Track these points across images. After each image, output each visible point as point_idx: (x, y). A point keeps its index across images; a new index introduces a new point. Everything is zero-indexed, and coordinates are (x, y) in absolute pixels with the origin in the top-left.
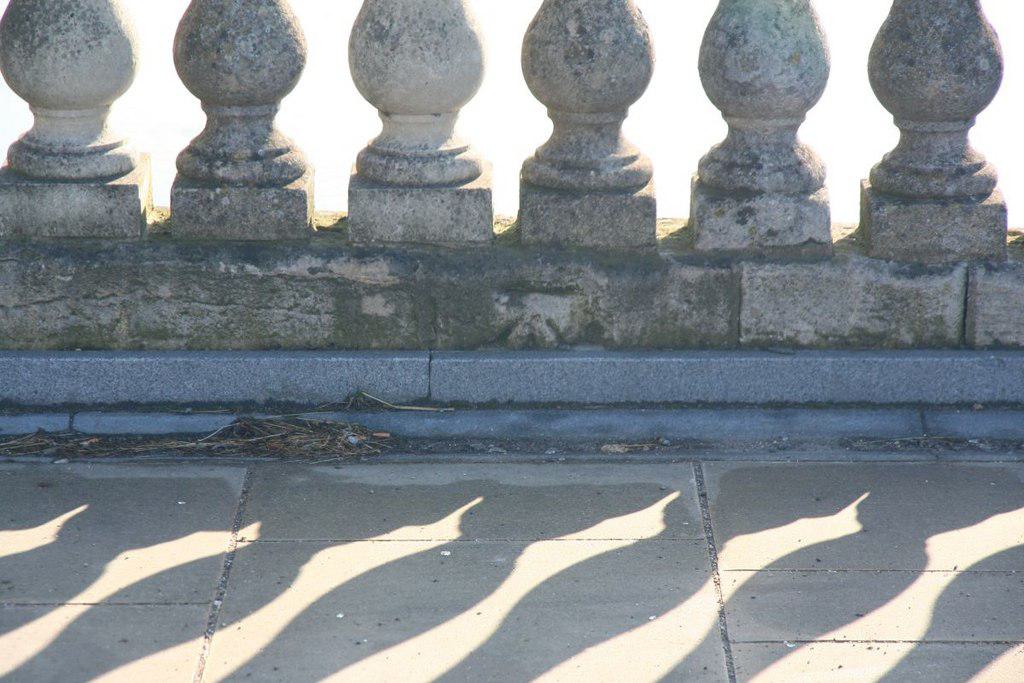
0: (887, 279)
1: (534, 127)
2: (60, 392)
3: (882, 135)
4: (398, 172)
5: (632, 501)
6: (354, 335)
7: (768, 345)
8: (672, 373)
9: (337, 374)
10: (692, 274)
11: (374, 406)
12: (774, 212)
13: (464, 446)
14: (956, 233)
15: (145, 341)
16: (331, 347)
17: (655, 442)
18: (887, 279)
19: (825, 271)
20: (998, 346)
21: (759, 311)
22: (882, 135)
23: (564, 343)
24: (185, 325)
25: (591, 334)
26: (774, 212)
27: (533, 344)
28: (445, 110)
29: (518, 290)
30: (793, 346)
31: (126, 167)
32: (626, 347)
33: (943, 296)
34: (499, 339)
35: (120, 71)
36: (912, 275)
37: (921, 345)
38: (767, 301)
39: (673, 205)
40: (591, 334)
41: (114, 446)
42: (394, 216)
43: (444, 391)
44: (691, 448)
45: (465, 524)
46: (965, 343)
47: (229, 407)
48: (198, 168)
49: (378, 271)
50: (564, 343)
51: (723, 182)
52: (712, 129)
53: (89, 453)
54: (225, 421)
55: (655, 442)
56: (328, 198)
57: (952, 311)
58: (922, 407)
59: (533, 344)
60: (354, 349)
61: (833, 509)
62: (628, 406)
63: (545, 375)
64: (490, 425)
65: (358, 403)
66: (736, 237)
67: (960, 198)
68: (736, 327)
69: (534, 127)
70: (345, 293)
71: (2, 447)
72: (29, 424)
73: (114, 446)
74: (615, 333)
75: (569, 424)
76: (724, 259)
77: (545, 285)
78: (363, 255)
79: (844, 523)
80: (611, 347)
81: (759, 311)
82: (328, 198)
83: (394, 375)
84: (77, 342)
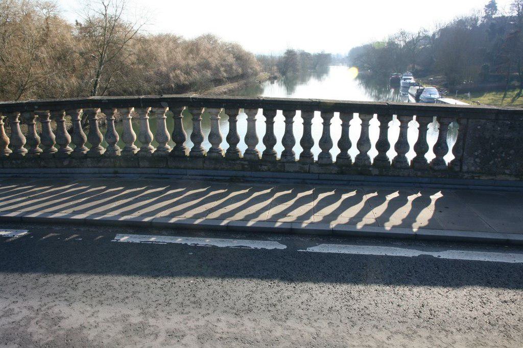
0: (301, 165)
1: (264, 148)
2: (212, 174)
3: (301, 150)
4: (249, 152)
5: (353, 190)
6: (243, 169)
7: (288, 172)
8: (277, 175)
9: (241, 173)
10: (280, 164)
11: (245, 177)
12: (289, 158)
13: (253, 182)
14: (308, 161)
15: (222, 169)
16: (241, 171)
17: (274, 182)
18: (301, 165)
19: (294, 164)
20: (312, 173)
21: (141, 164)
22: (301, 150)
23: (266, 171)
24: (226, 168)
25: (269, 170)
26: (289, 158)
27: (263, 171)
28: (255, 146)
29: (261, 165)
30: (291, 172)
31: (257, 152)
32: (273, 171)
33: (306, 167)
34: (259, 171)
35: (370, 147)
36: (303, 165)
37: (304, 173)
38: (288, 167)
39: (279, 156)
40: (269, 170)
41: (217, 180)
42: (248, 157)
43: (63, 172)
44: (278, 183)
45: (335, 192)
46: (309, 172)
47: (230, 176)
48: (265, 153)
49: (246, 163)
50: (266, 171)
51: (284, 154)
52: (283, 149)
53: (214, 181)
54: (229, 178)
55: (274, 182)
56: (242, 154)
57: (308, 170)
58: (304, 179)
59: (263, 171)
60: (244, 171)
61: (289, 190)
62: (272, 178)
63: (264, 174)
64: (256, 179)
65: (244, 176)
66: (285, 160)
67: (309, 157)
68: (284, 170)
69: (264, 148)
70: (243, 165)
71: (1, 177)
72: (209, 178)
73: (217, 180)
74: (271, 170)
75: (265, 180)
76: (284, 162)
77: (359, 169)
78: (245, 161)
79: (333, 193)
80: (271, 172)
81: (287, 168)
82: (242, 154)
83: (247, 174)
84: (215, 169)
